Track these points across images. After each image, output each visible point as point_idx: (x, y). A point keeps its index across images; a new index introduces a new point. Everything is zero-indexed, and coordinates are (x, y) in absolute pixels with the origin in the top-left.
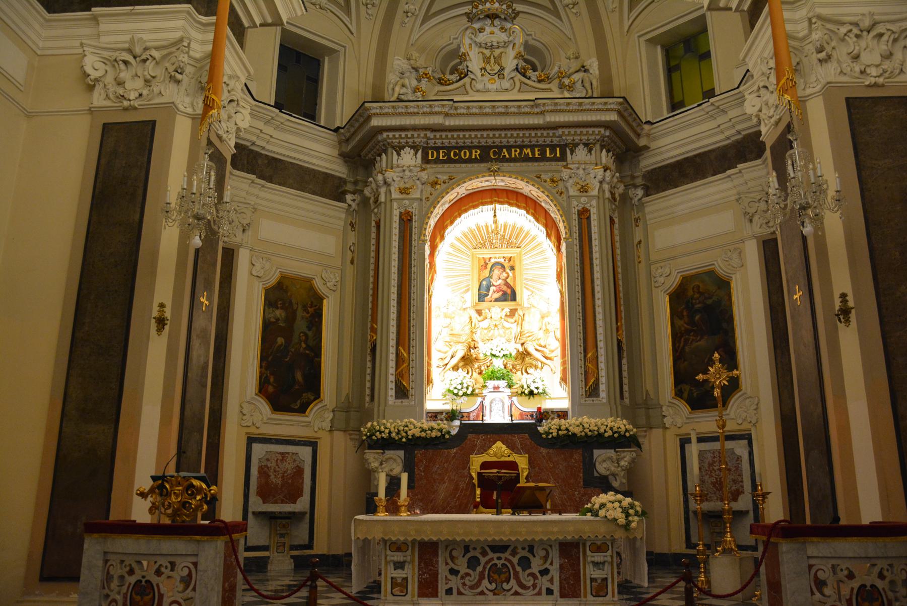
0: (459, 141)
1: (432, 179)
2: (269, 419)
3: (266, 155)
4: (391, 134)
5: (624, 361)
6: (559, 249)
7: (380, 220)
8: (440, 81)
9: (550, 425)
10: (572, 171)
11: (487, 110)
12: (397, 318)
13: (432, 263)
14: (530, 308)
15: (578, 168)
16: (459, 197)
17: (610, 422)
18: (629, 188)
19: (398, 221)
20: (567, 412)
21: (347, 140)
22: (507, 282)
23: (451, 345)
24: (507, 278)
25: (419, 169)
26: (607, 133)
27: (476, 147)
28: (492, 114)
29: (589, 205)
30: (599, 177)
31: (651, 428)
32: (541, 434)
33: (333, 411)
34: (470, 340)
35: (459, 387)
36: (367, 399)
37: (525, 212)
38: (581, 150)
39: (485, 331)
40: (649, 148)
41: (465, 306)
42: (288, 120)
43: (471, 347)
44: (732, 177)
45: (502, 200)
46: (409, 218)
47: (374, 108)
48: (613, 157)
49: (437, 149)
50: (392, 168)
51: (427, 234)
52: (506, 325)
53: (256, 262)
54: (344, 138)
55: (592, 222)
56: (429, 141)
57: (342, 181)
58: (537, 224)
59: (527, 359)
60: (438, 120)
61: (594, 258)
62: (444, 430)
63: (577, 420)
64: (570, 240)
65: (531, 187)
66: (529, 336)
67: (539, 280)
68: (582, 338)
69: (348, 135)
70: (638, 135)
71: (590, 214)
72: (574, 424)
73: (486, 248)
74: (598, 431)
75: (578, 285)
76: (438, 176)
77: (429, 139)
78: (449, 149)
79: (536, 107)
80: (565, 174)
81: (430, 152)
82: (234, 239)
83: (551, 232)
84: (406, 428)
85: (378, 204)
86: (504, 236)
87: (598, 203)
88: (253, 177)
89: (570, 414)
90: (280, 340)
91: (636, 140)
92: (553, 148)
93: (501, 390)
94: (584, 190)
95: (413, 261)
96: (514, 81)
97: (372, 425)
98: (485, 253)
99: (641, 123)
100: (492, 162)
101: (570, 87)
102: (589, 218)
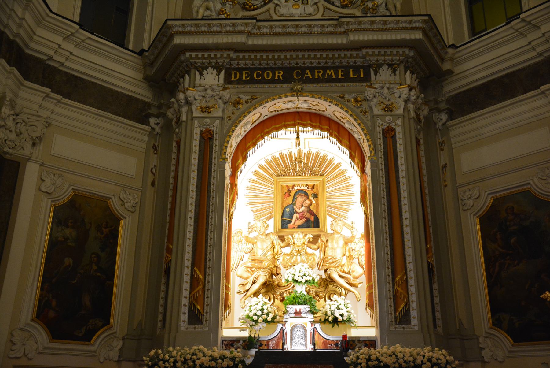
0: (262, 62)
1: (234, 98)
2: (45, 348)
3: (66, 73)
4: (194, 54)
5: (435, 286)
6: (363, 170)
7: (180, 140)
8: (244, 6)
9: (358, 354)
10: (376, 91)
11: (291, 30)
12: (194, 237)
13: (233, 185)
14: (334, 233)
15: (382, 88)
16: (262, 119)
17: (426, 351)
18: (433, 113)
19: (198, 140)
20: (375, 341)
21: (152, 64)
22: (310, 209)
23: (252, 271)
24: (310, 205)
25: (222, 88)
26: (412, 54)
27: (279, 69)
28: (295, 33)
29: (394, 124)
30: (404, 96)
31: (468, 362)
32: (348, 365)
33: (123, 339)
34: (272, 266)
35: (259, 313)
36: (159, 325)
37: (328, 134)
38: (385, 70)
39: (288, 258)
40: (453, 72)
41: (267, 232)
42: (90, 38)
43: (274, 273)
44: (547, 92)
45: (305, 123)
46: (210, 136)
47: (176, 26)
48: (417, 80)
49: (241, 70)
50: (194, 87)
51: (228, 152)
52: (310, 251)
53: (46, 177)
54: (148, 61)
55: (398, 141)
56: (232, 62)
57: (147, 105)
58: (340, 146)
59: (331, 286)
60: (240, 39)
61: (401, 177)
62: (237, 359)
63: (388, 349)
64: (375, 158)
65: (335, 108)
66: (332, 263)
67: (341, 206)
68: (389, 260)
69: (152, 58)
70: (442, 60)
71: (395, 132)
72: (386, 354)
73: (290, 176)
74: (414, 362)
75: (384, 204)
76: (241, 96)
77: (232, 59)
78: (252, 70)
79: (340, 27)
80: (369, 93)
81: (233, 73)
82: (22, 151)
83: (355, 153)
84: (194, 357)
85: (179, 123)
86: (307, 164)
87: (403, 122)
88: (48, 90)
89: (379, 343)
90: (68, 261)
91: (440, 64)
92: (357, 69)
93: (303, 315)
94: (388, 109)
95: (212, 179)
96: (317, 6)
97: (156, 353)
98: (288, 181)
99: (445, 47)
100: (295, 82)
101: (373, 10)
102: (394, 137)
